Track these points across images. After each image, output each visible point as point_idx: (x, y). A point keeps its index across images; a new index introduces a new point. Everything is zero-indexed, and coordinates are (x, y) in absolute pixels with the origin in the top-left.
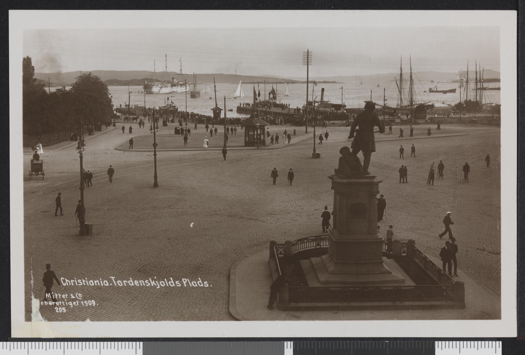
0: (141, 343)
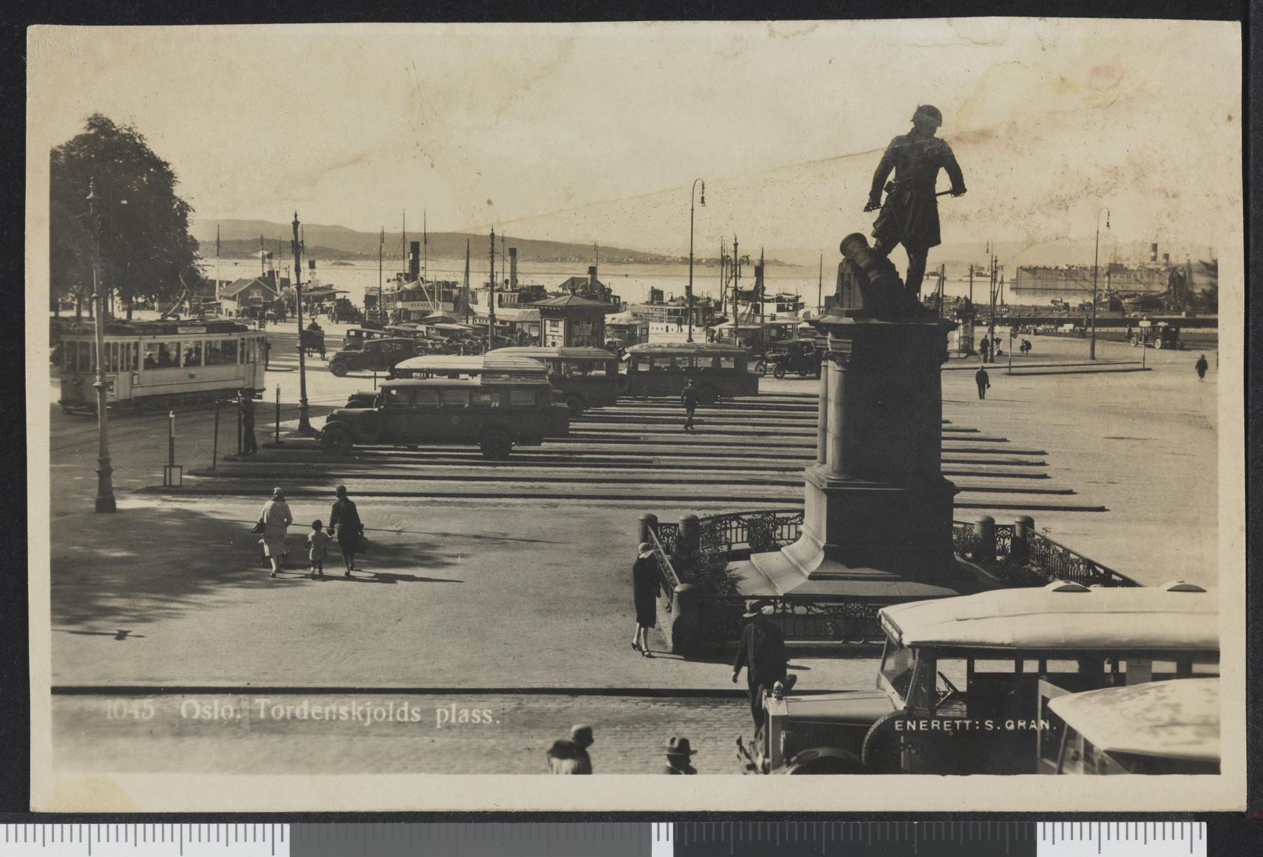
0: (287, 827)
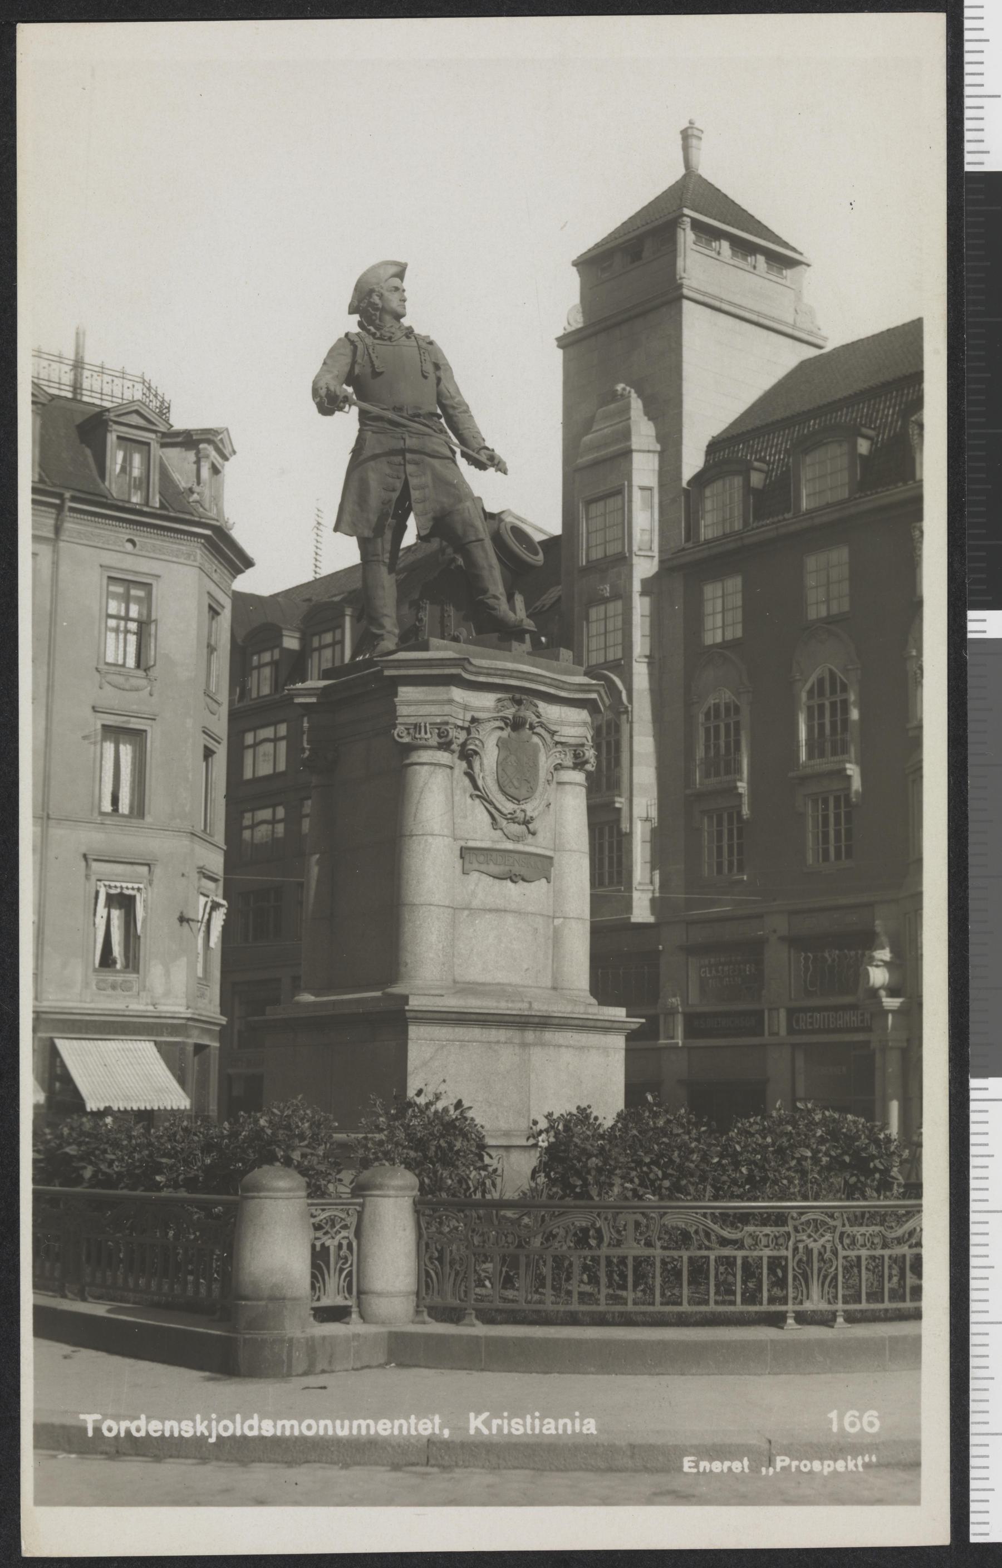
0: (974, 1083)
